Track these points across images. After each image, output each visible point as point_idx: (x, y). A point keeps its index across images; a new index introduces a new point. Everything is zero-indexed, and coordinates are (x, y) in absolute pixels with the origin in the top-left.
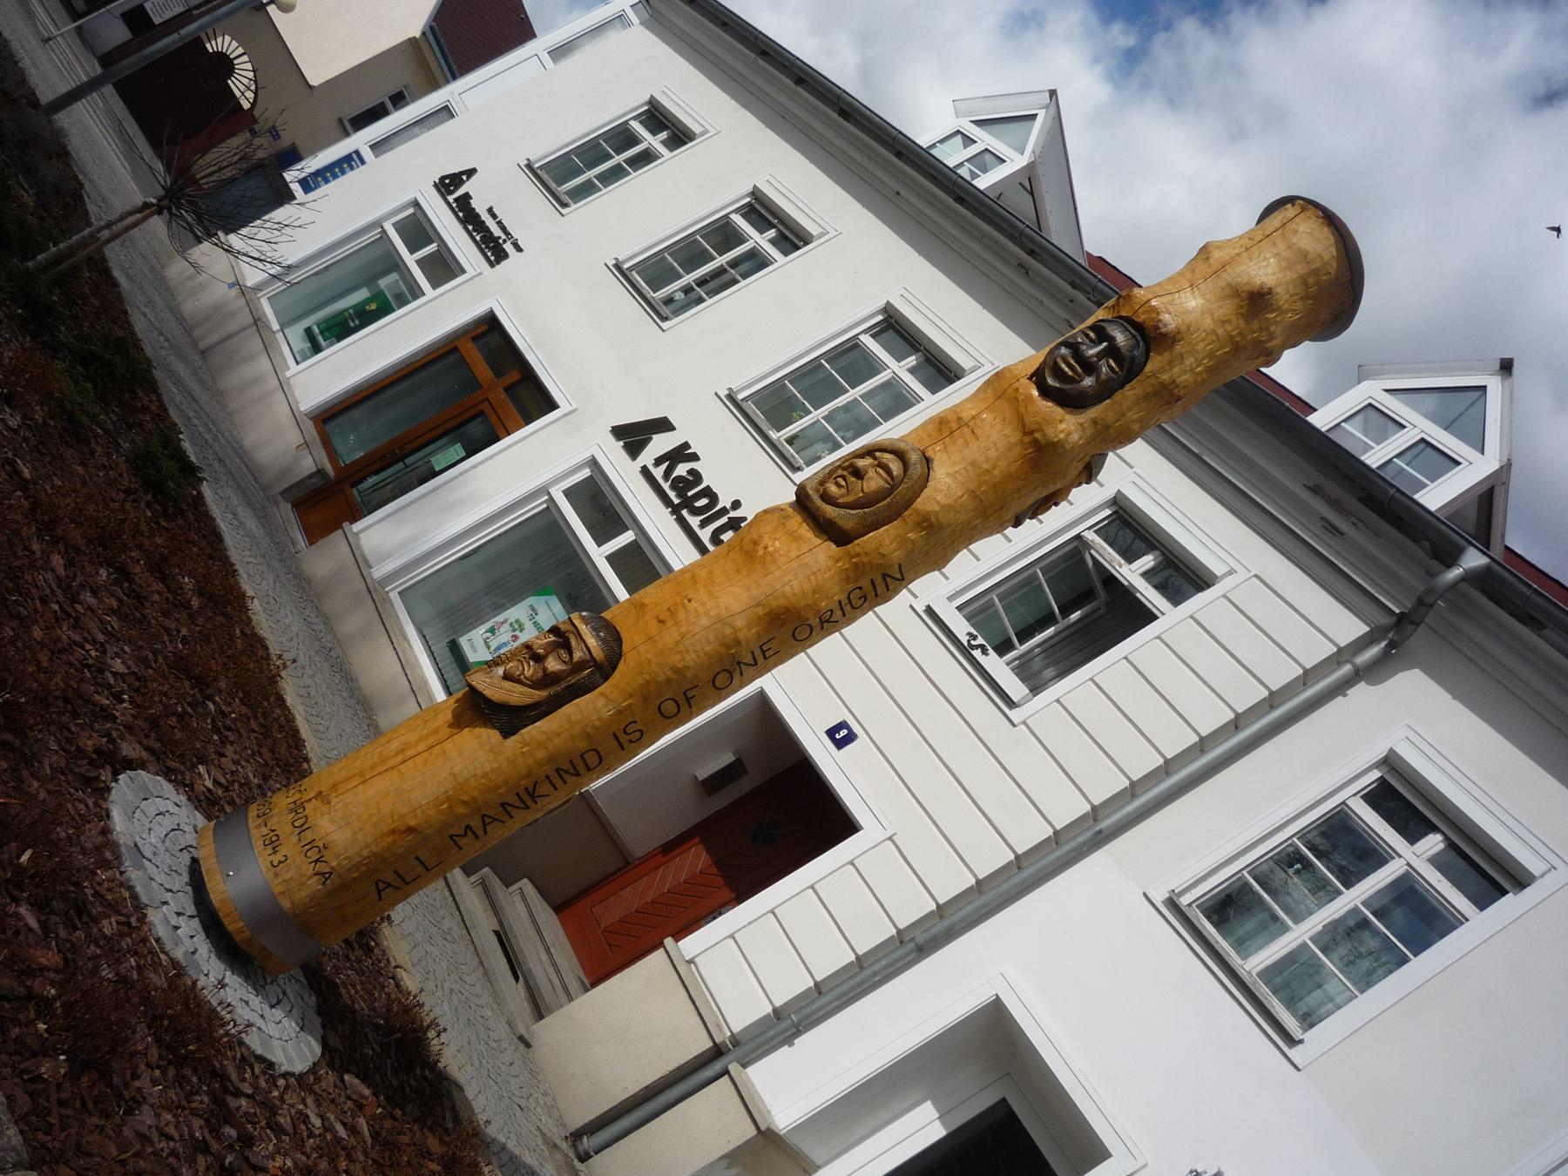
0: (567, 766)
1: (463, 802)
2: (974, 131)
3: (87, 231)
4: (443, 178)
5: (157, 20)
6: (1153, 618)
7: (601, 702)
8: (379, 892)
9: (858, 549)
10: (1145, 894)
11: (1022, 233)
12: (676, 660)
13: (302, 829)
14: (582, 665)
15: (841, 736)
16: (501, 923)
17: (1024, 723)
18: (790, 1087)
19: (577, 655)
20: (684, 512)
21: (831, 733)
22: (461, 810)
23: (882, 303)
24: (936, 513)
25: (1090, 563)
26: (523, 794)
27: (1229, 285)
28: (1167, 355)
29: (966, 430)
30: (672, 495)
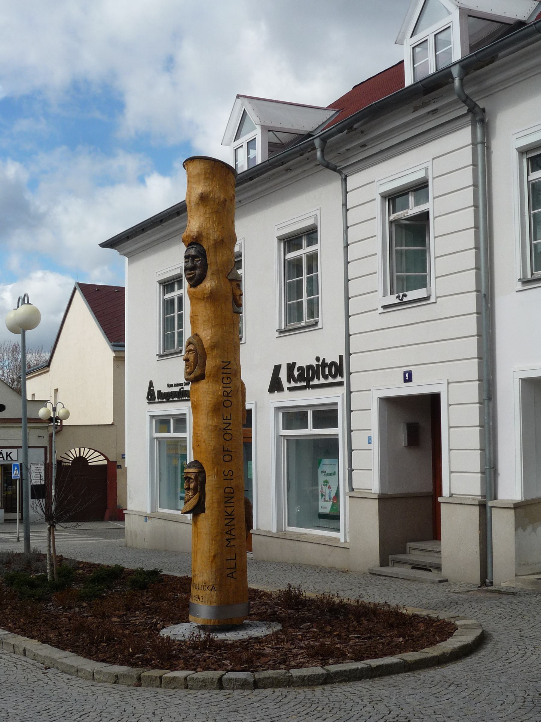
0: (226, 499)
1: (217, 536)
2: (238, 142)
3: (48, 556)
4: (148, 397)
5: (43, 483)
6: (428, 212)
7: (210, 478)
8: (232, 577)
9: (208, 373)
10: (517, 291)
11: (270, 164)
12: (210, 448)
13: (198, 587)
14: (196, 477)
15: (408, 377)
16: (410, 564)
17: (437, 297)
18: (511, 487)
19: (193, 477)
20: (311, 383)
21: (405, 381)
22: (218, 538)
23: (276, 240)
24: (211, 342)
25: (407, 222)
26: (226, 517)
27: (195, 205)
28: (205, 239)
29: (195, 317)
30: (299, 384)
